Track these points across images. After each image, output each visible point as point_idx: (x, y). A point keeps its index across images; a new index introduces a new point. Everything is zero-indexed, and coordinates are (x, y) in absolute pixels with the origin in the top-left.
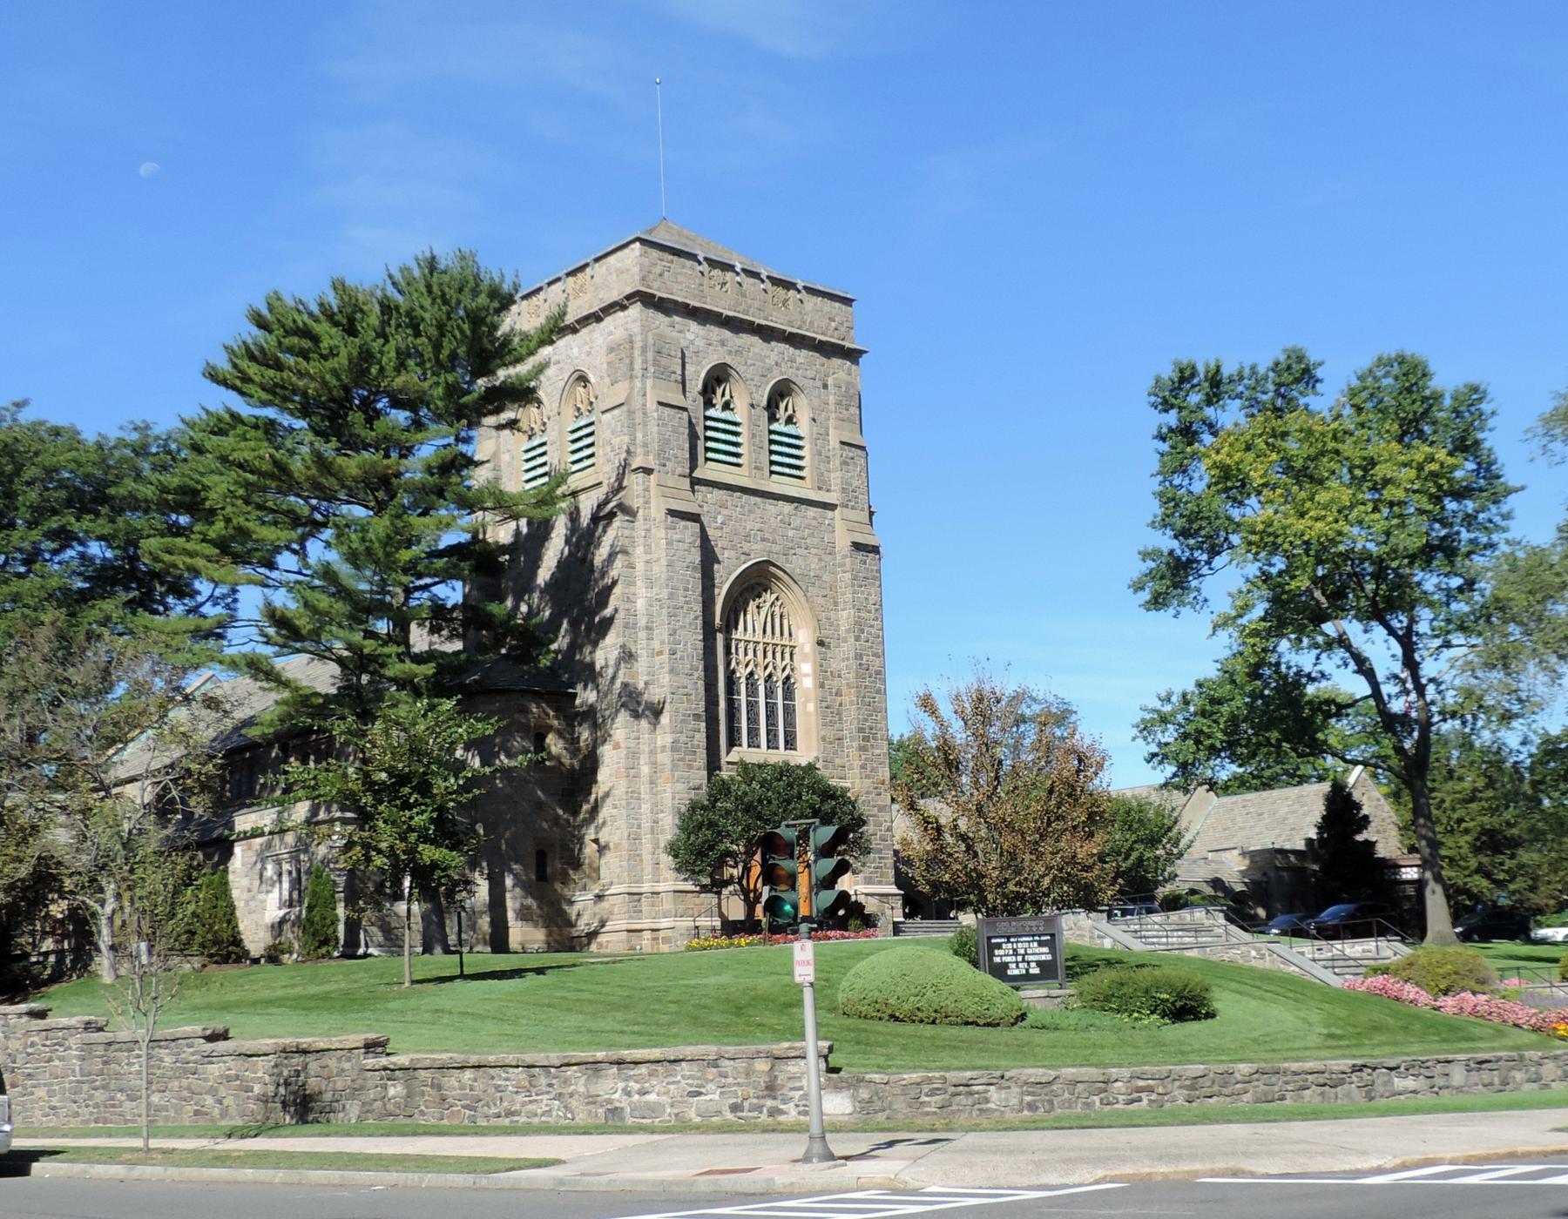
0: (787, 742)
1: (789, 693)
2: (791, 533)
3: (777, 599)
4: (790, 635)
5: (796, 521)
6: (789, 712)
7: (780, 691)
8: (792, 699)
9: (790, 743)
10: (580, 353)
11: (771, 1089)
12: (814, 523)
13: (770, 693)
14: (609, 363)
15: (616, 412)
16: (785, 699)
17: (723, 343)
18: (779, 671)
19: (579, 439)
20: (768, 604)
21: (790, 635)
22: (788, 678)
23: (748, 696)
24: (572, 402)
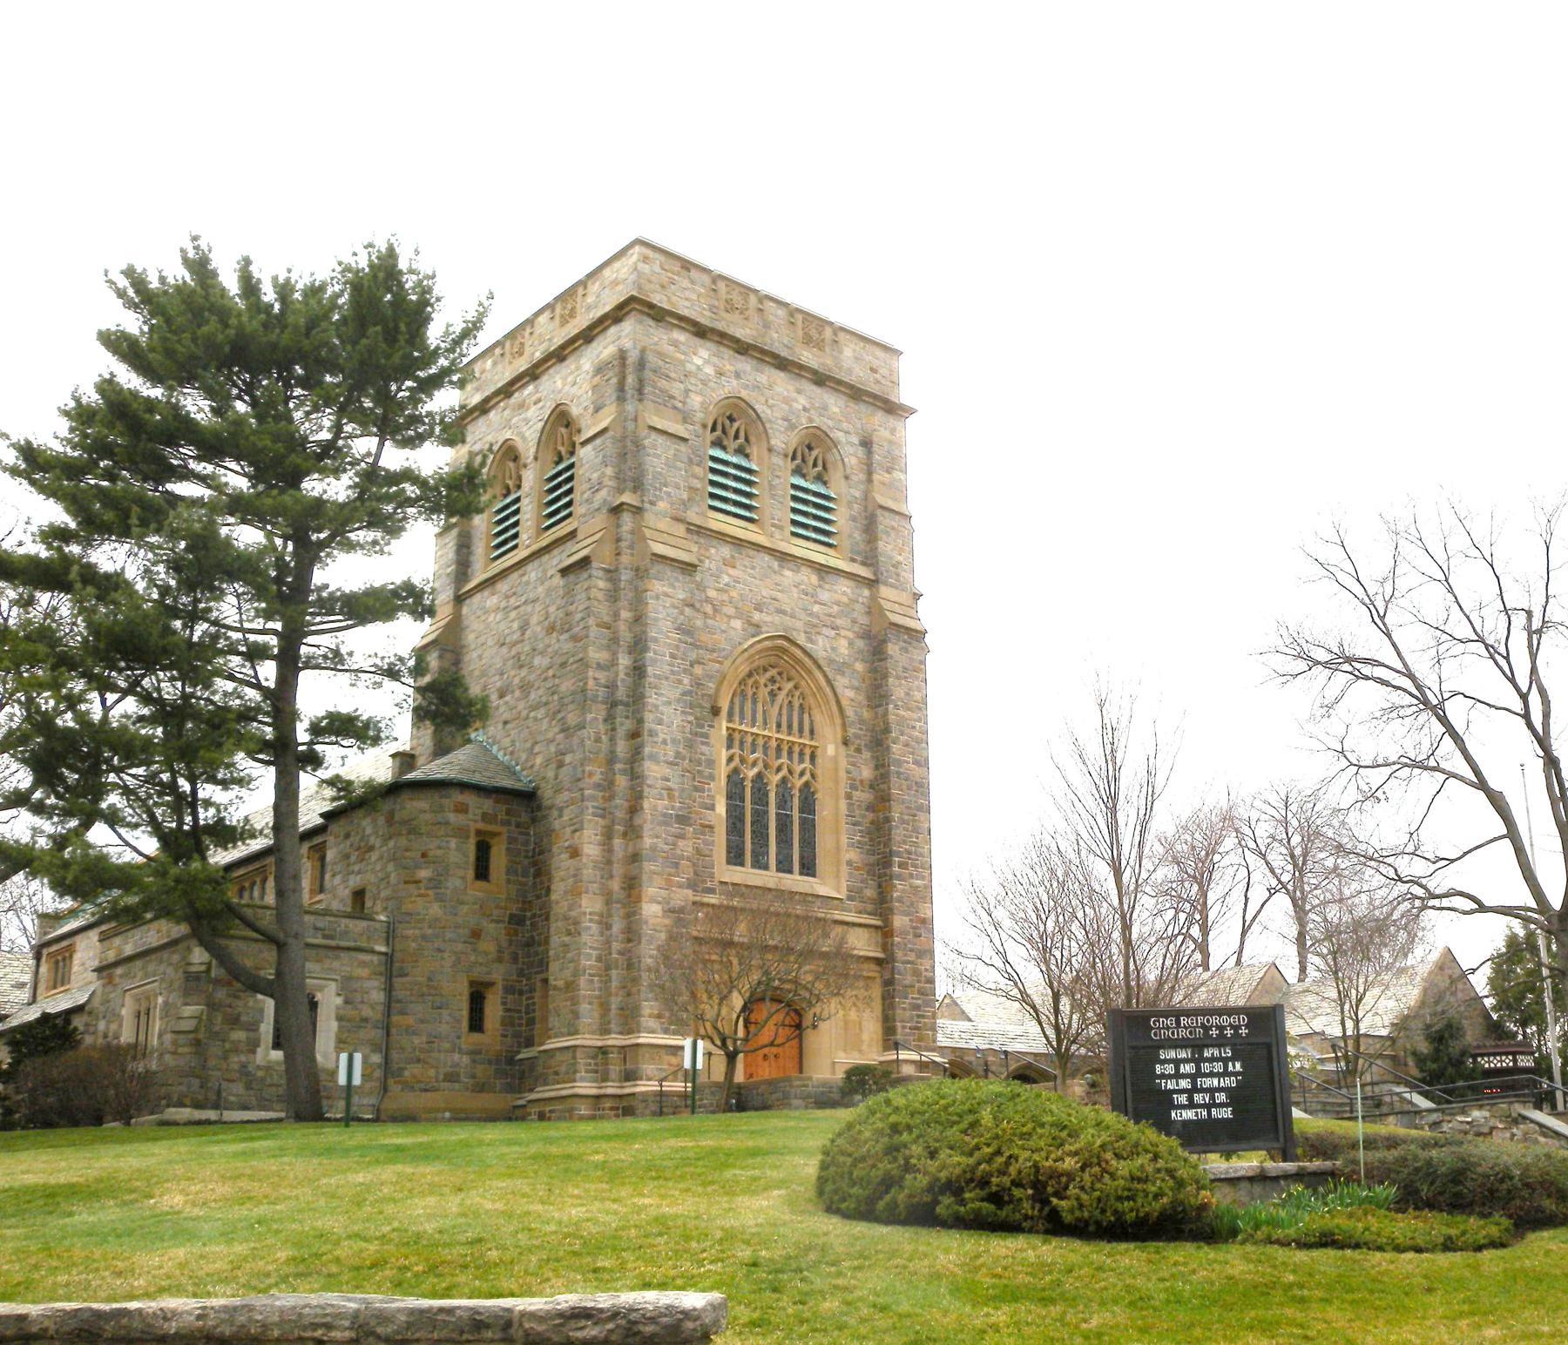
0: (779, 862)
1: (808, 804)
2: (816, 608)
3: (796, 687)
4: (812, 732)
5: (825, 596)
6: (808, 827)
7: (796, 801)
8: (813, 812)
9: (808, 868)
10: (564, 385)
11: (784, 1224)
12: (845, 599)
13: (783, 802)
14: (595, 388)
15: (598, 441)
16: (801, 811)
17: (738, 375)
18: (796, 775)
19: (559, 486)
20: (784, 692)
21: (812, 732)
22: (807, 784)
23: (766, 812)
24: (551, 446)
